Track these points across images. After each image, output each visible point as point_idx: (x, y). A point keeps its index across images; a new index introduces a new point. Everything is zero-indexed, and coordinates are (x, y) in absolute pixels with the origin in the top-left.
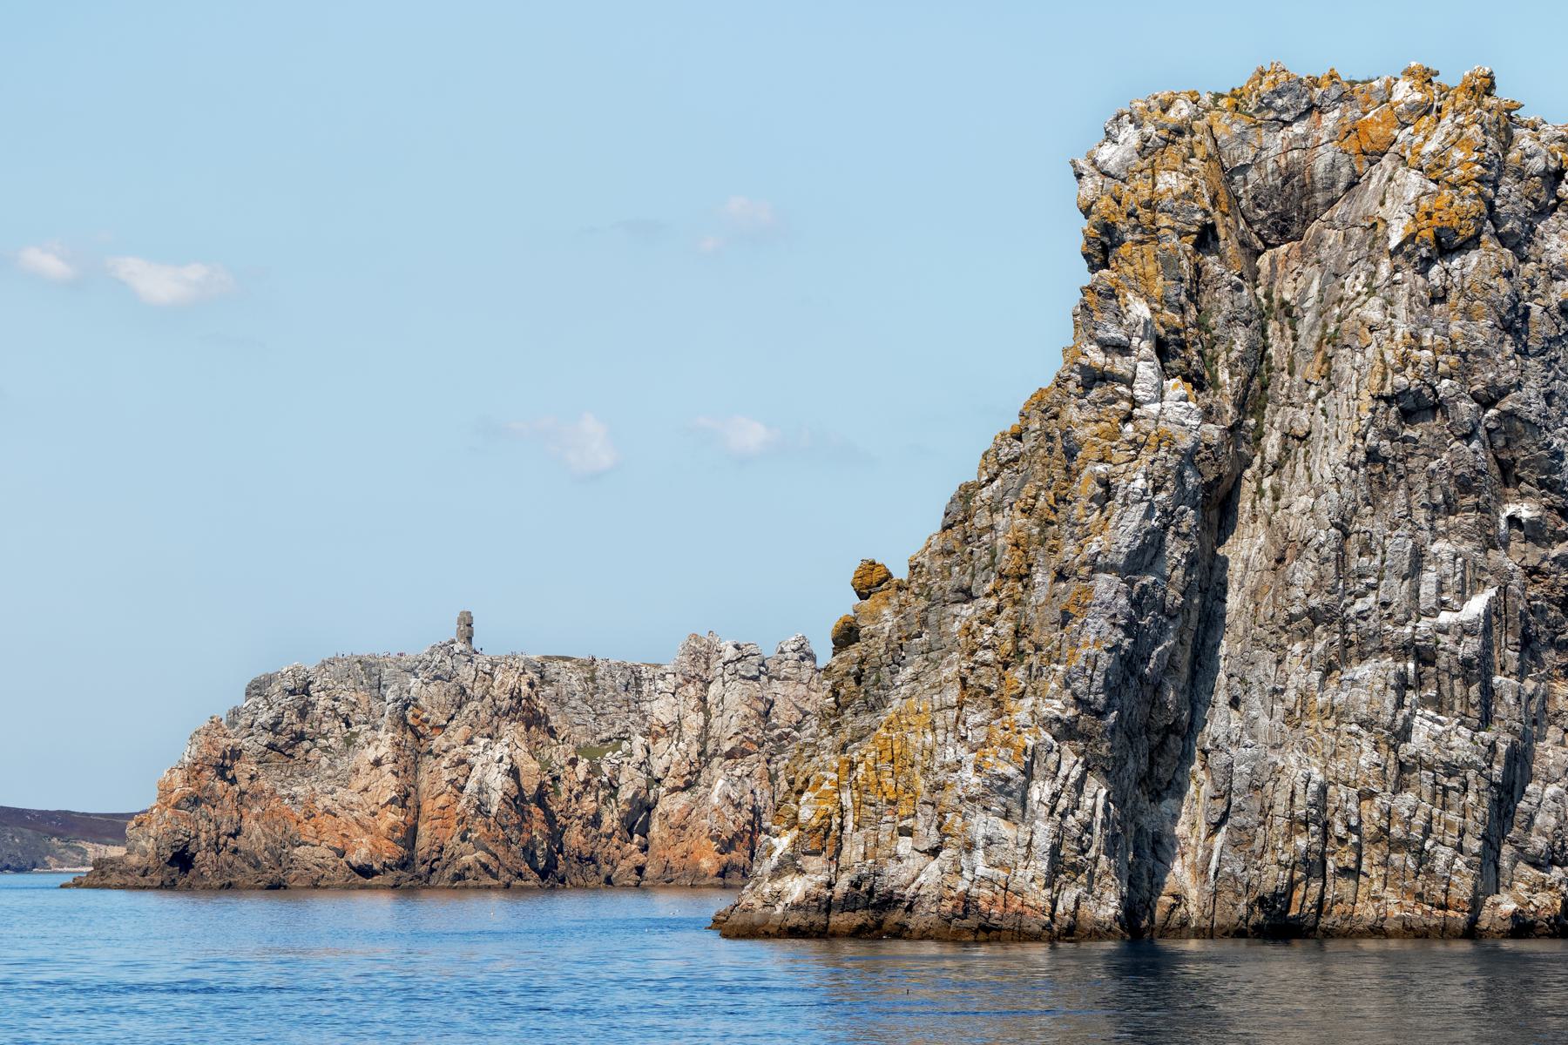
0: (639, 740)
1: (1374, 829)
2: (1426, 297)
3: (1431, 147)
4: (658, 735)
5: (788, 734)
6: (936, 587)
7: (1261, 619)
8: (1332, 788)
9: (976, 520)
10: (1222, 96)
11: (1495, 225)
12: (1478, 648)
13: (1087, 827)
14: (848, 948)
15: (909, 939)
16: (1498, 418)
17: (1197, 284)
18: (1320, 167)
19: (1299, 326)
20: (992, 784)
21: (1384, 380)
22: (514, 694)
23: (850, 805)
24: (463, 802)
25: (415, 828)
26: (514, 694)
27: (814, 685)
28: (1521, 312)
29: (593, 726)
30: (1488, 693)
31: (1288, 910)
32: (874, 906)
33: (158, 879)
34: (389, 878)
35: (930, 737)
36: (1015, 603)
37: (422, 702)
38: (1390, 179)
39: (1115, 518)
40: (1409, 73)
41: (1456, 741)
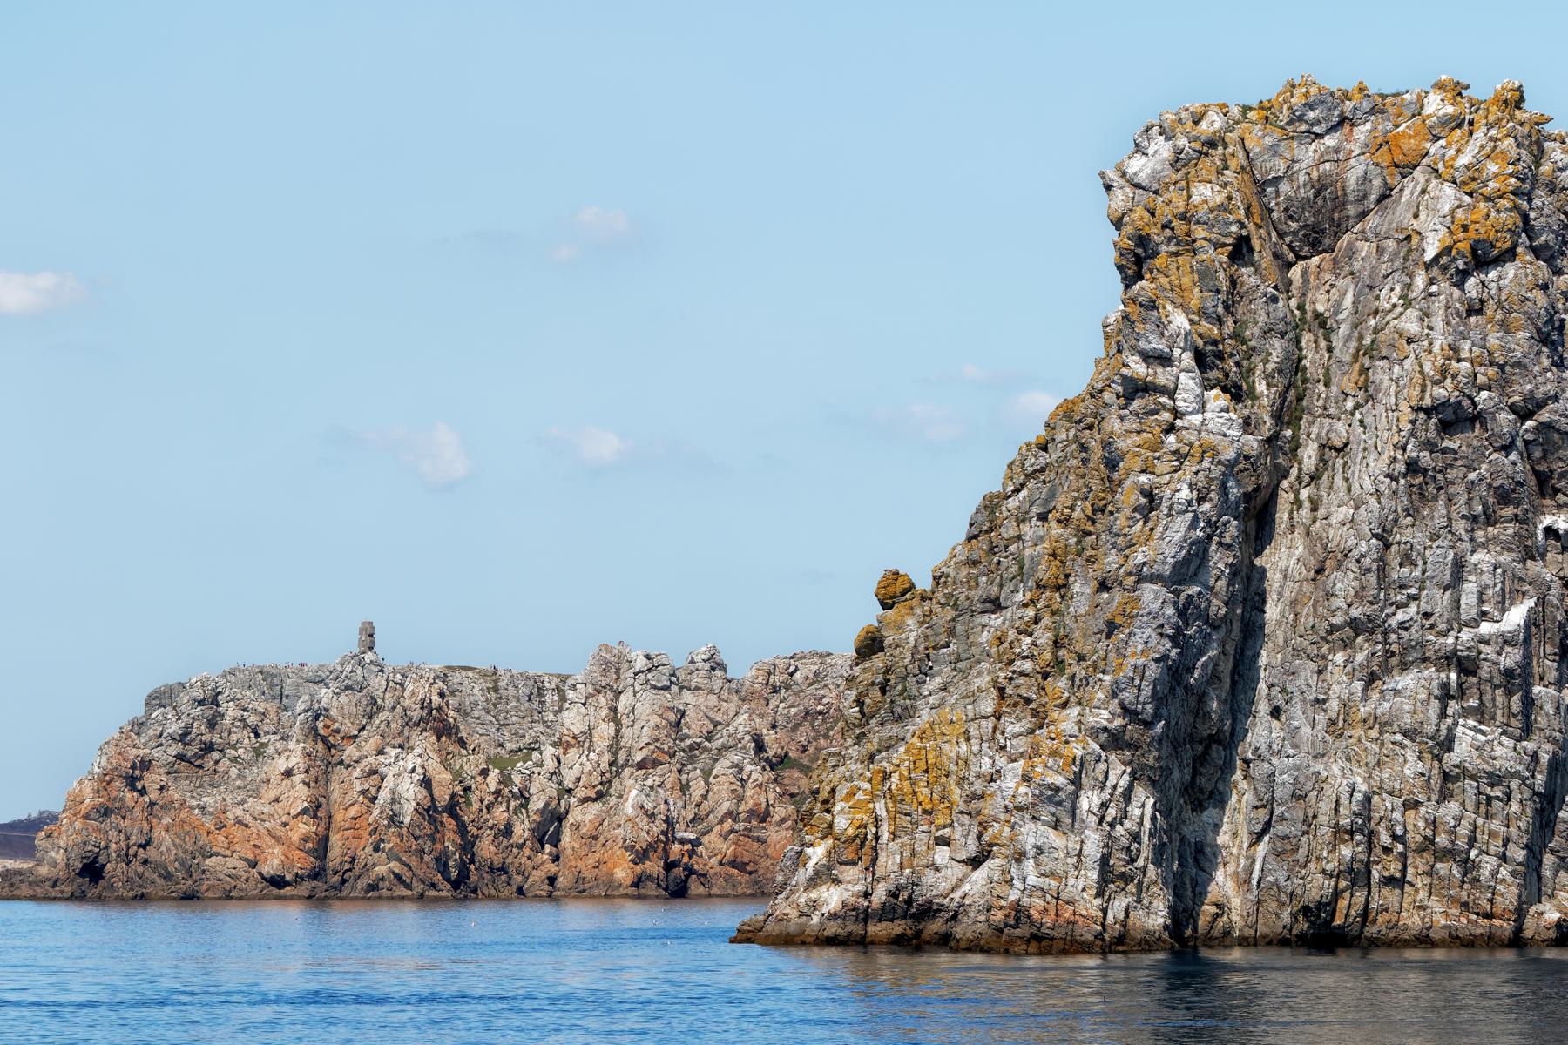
0: (549, 751)
1: (1419, 839)
2: (1462, 310)
3: (1464, 160)
4: (569, 745)
5: (699, 744)
6: (962, 597)
7: (1301, 629)
8: (1376, 797)
9: (1002, 530)
10: (1251, 109)
11: (1530, 238)
12: (1519, 658)
13: (1135, 837)
14: (884, 959)
15: (955, 950)
16: (1536, 430)
17: (1234, 294)
18: (1352, 179)
19: (1334, 338)
20: (1041, 794)
21: (1423, 391)
22: (425, 705)
23: (884, 814)
24: (376, 812)
25: (326, 839)
26: (425, 705)
27: (725, 695)
28: (1557, 324)
29: (496, 736)
30: (1529, 702)
31: (1333, 920)
32: (913, 916)
33: (68, 890)
34: (304, 889)
35: (964, 747)
36: (1053, 613)
37: (334, 712)
38: (1423, 192)
39: (1160, 529)
40: (1440, 86)
41: (1499, 751)
